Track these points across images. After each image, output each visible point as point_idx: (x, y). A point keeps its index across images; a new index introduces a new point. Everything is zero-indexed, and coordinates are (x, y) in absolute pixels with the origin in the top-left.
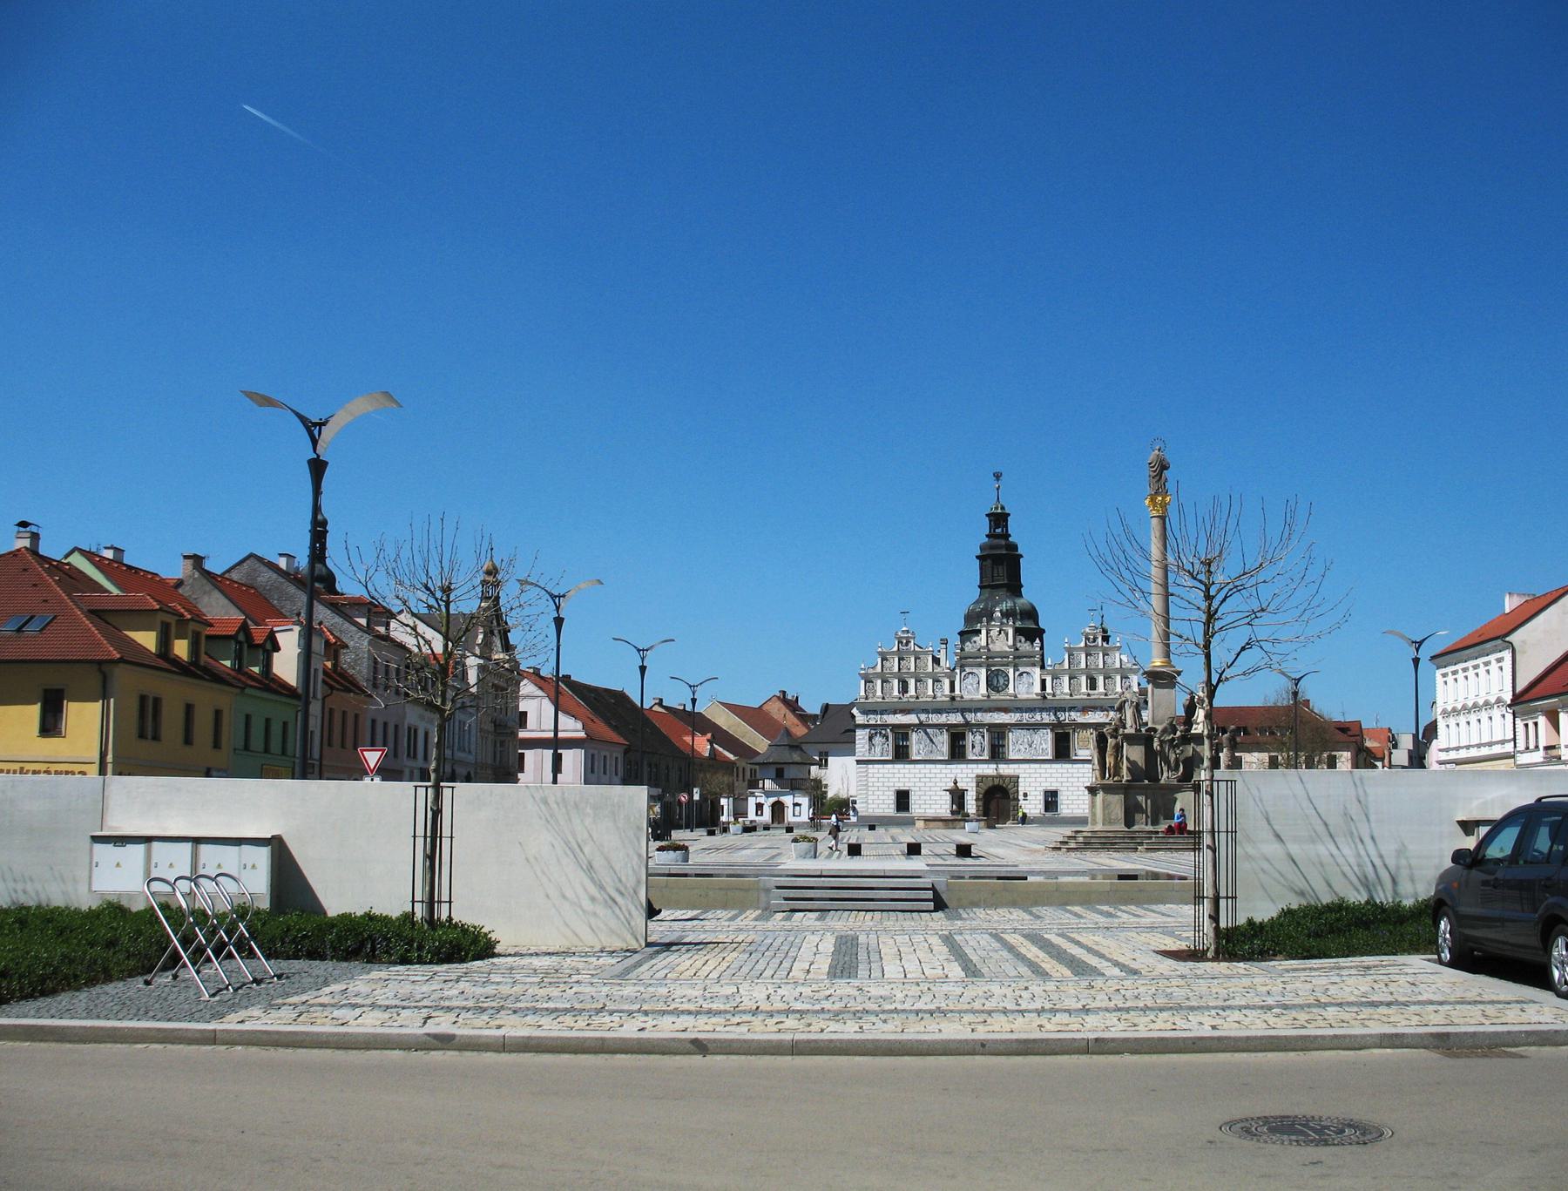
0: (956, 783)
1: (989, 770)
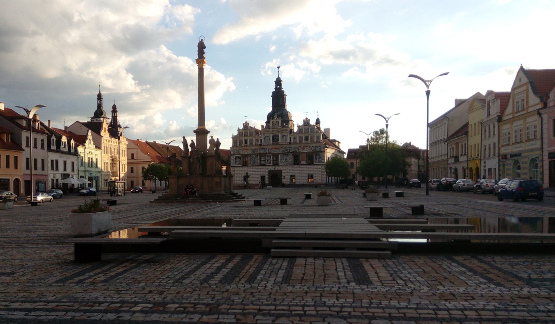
0: (247, 173)
1: (272, 168)
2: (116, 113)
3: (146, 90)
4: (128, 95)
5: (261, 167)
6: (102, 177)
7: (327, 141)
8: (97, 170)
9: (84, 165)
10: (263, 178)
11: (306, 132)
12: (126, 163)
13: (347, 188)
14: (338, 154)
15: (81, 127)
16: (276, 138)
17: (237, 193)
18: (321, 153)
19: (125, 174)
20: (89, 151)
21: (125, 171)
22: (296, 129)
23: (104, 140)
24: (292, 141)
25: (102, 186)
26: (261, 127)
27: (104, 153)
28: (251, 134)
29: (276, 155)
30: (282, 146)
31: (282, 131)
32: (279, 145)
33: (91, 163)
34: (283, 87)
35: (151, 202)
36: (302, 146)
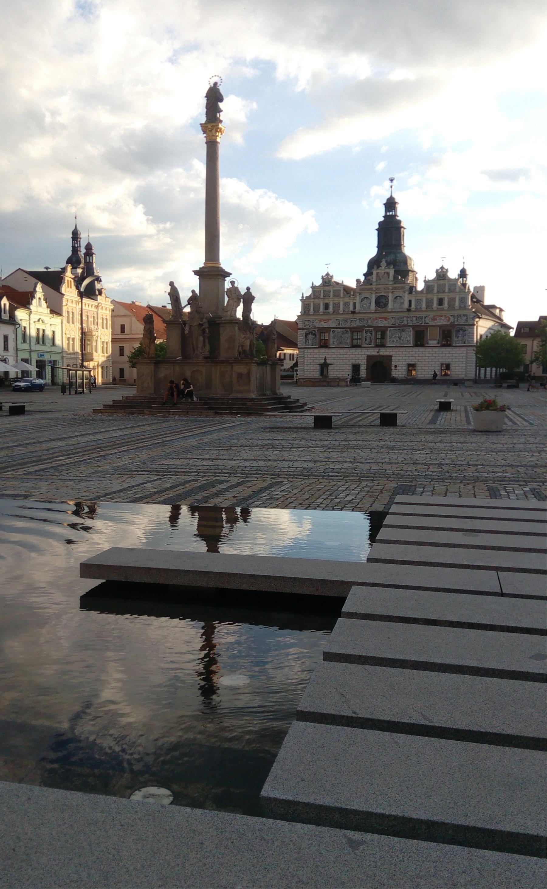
0: (325, 359)
1: (373, 352)
2: (91, 257)
3: (166, 231)
4: (137, 240)
5: (353, 350)
6: (63, 362)
7: (481, 307)
8: (53, 349)
9: (28, 341)
10: (356, 368)
11: (441, 290)
12: (110, 340)
13: (516, 386)
14: (499, 328)
15: (26, 279)
16: (383, 300)
17: (289, 397)
18: (467, 327)
19: (108, 357)
20: (38, 318)
21: (107, 353)
22: (420, 286)
23: (67, 301)
24: (413, 306)
25: (63, 376)
26: (356, 283)
27: (68, 322)
28: (337, 294)
29: (383, 331)
30: (393, 315)
31: (395, 288)
32: (388, 312)
33: (41, 339)
34: (398, 214)
35: (95, 411)
36: (431, 314)
